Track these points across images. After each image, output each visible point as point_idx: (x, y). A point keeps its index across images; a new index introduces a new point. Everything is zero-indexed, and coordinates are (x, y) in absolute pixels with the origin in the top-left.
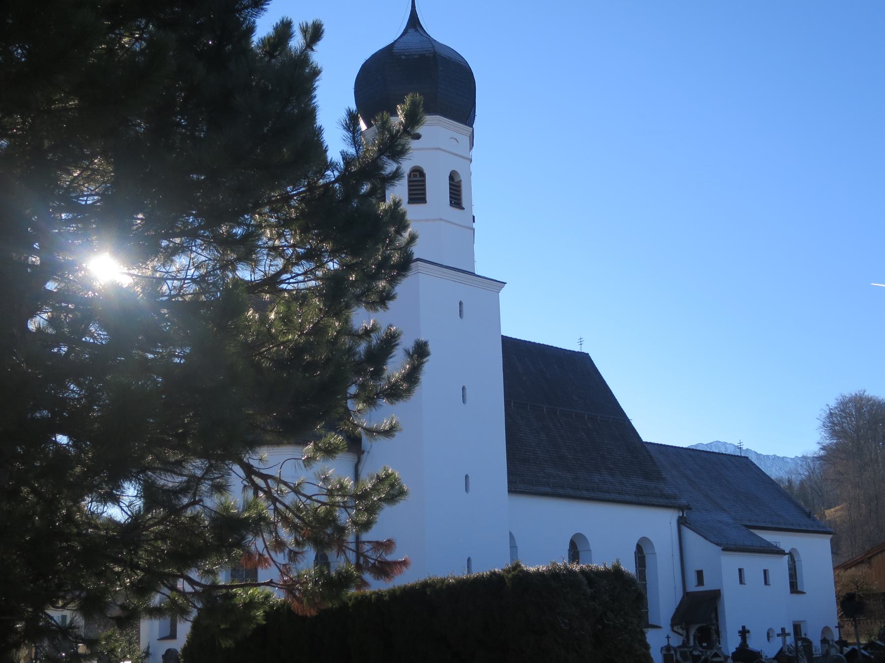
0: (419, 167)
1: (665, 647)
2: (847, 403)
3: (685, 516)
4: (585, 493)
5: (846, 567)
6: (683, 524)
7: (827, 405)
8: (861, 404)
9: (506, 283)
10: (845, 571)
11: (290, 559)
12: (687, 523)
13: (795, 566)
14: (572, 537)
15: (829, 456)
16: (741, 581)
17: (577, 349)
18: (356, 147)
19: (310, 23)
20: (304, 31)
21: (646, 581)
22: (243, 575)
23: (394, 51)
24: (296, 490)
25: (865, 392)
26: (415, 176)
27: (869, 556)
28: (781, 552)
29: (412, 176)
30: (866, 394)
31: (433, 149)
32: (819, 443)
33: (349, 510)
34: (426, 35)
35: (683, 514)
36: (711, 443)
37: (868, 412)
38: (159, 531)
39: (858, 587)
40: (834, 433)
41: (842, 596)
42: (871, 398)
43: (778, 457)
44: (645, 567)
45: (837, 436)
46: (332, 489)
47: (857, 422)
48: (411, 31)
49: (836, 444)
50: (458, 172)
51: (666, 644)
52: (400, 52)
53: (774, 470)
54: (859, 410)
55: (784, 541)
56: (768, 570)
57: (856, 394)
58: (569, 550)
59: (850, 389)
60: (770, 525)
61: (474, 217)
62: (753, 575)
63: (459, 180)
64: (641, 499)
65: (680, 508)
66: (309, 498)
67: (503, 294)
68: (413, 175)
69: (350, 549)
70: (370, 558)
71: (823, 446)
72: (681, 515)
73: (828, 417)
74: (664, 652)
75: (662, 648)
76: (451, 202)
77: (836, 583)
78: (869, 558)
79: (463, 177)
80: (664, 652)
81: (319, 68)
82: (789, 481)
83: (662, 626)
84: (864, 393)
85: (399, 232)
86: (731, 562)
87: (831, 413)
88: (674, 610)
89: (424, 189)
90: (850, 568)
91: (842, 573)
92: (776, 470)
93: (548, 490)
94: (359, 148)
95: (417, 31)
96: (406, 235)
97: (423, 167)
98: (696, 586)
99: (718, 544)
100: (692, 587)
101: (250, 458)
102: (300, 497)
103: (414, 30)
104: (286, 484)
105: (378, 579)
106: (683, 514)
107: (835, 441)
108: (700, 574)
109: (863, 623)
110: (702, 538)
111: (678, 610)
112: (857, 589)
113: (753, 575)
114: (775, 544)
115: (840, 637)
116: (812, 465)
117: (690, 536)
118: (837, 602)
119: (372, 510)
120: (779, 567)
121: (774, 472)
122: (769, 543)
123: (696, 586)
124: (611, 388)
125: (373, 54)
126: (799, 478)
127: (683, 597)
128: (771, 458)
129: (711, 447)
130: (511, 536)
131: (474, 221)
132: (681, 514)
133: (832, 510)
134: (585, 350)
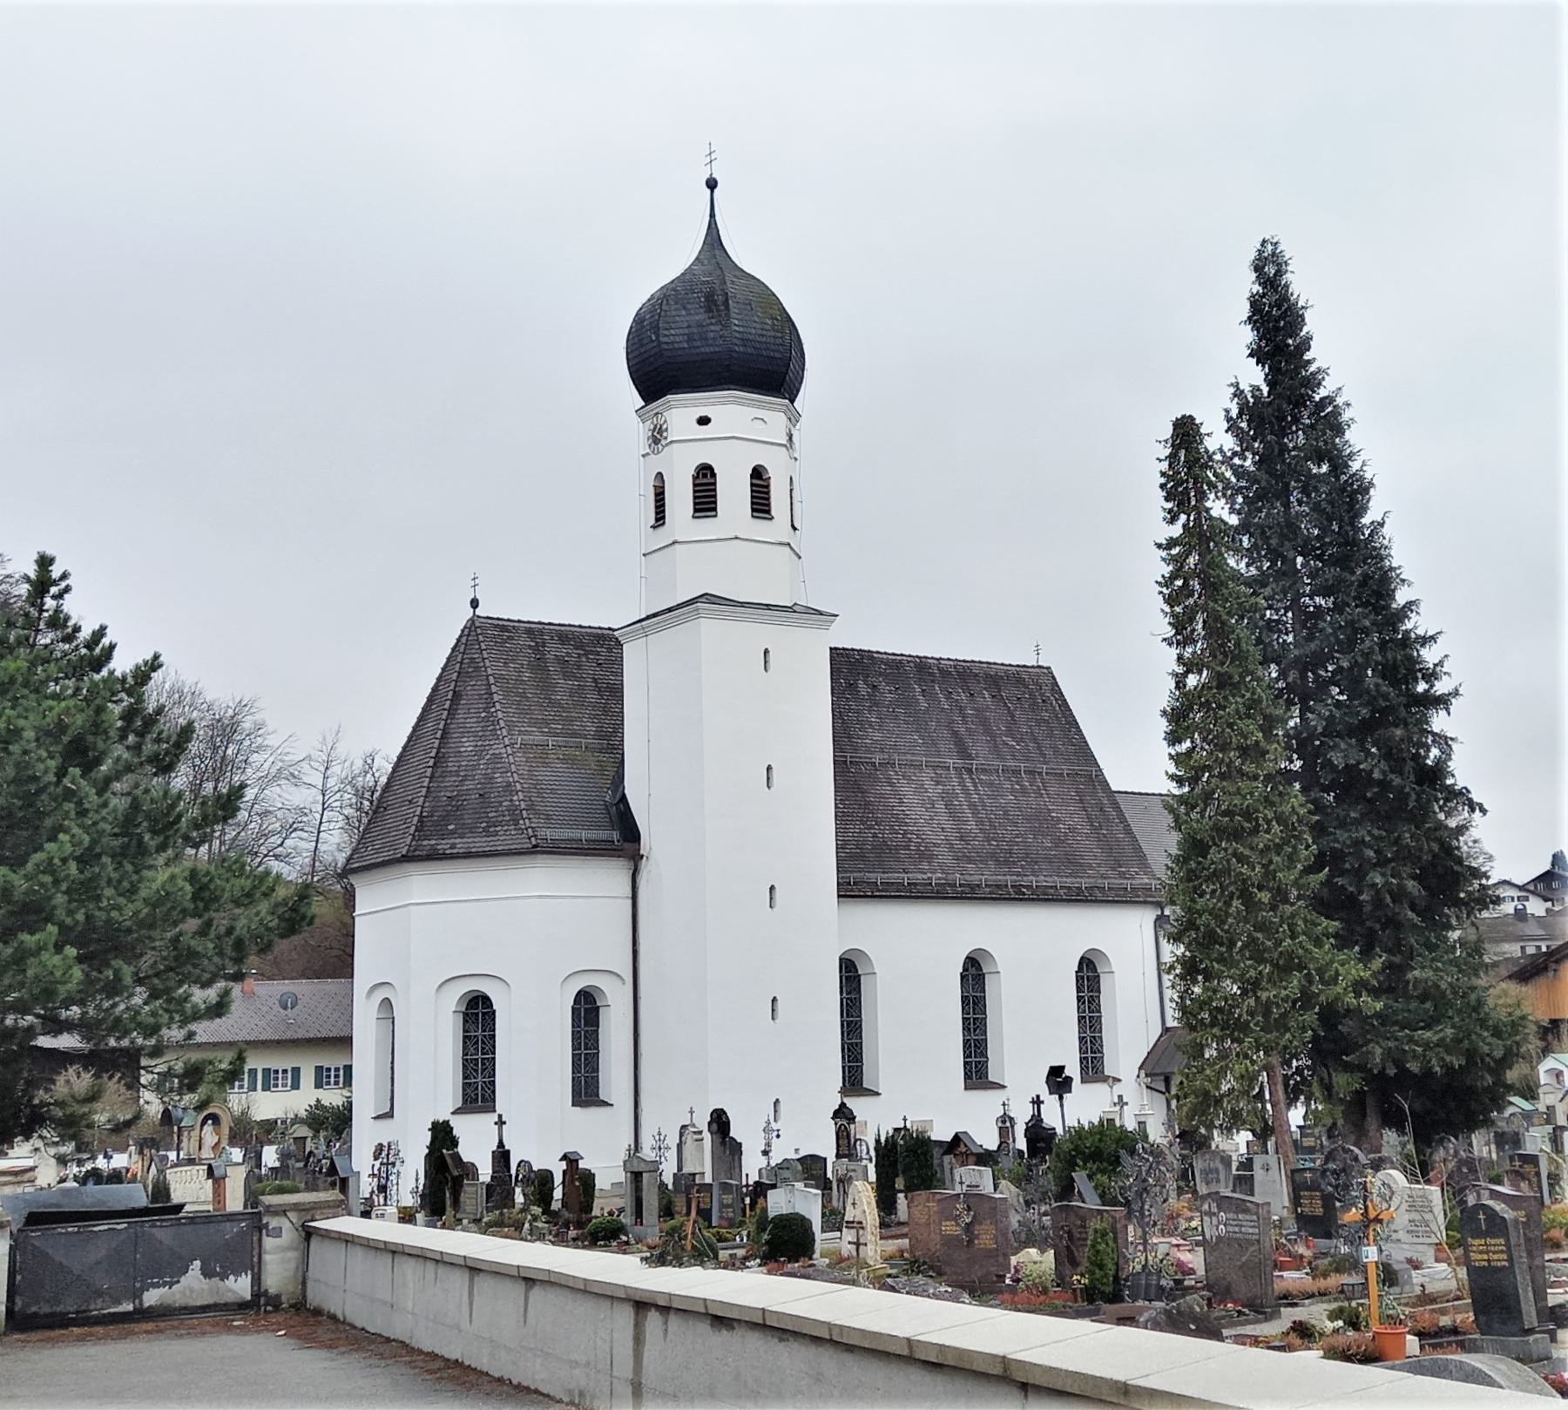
9: (837, 616)
17: (1030, 661)
72: (1159, 913)
132: (1159, 913)
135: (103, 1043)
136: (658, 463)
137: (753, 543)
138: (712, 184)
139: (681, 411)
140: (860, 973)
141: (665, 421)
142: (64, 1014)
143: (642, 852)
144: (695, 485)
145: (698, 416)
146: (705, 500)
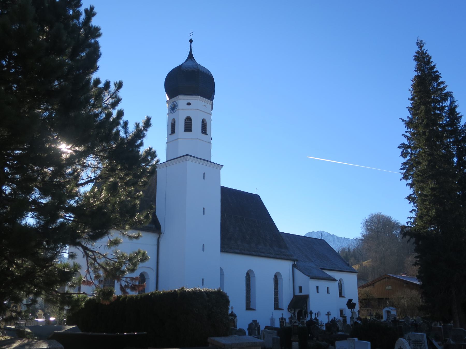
0: (190, 117)
1: (281, 318)
2: (373, 217)
3: (295, 263)
4: (254, 253)
5: (363, 287)
6: (294, 267)
7: (365, 218)
8: (379, 218)
9: (223, 166)
10: (363, 289)
11: (99, 283)
12: (296, 266)
13: (341, 286)
14: (248, 271)
15: (366, 239)
16: (318, 292)
17: (254, 193)
18: (126, 134)
19: (118, 81)
20: (115, 84)
21: (278, 290)
22: (109, 283)
23: (181, 68)
24: (104, 257)
25: (381, 213)
26: (188, 120)
27: (373, 283)
28: (335, 280)
29: (186, 120)
30: (382, 214)
31: (195, 109)
32: (361, 233)
33: (126, 264)
34: (195, 62)
35: (295, 263)
36: (318, 232)
37: (382, 221)
38: (448, 117)
39: (368, 295)
40: (368, 230)
41: (361, 299)
42: (384, 215)
43: (346, 239)
44: (278, 284)
45: (369, 231)
46: (119, 257)
47: (378, 225)
48: (189, 60)
49: (368, 234)
50: (206, 119)
51: (281, 317)
52: (184, 69)
53: (344, 243)
54: (378, 220)
55: (337, 275)
56: (329, 287)
57: (377, 214)
58: (246, 277)
59: (375, 211)
60: (331, 269)
61: (211, 138)
62: (323, 289)
63: (206, 122)
64: (278, 256)
65: (293, 260)
66: (110, 259)
67: (222, 170)
68: (187, 120)
69: (123, 280)
70: (129, 283)
71: (363, 235)
72: (294, 263)
73: (366, 223)
74: (280, 320)
75: (280, 319)
76: (202, 132)
77: (359, 293)
78: (374, 283)
79: (207, 121)
80: (280, 320)
81: (121, 98)
82: (349, 249)
83: (284, 309)
84: (381, 214)
85: (152, 159)
86: (313, 284)
87: (367, 221)
88: (289, 303)
89: (191, 126)
90: (365, 287)
91: (362, 289)
92: (345, 244)
93: (238, 251)
94: (127, 135)
95: (191, 60)
96: (156, 159)
97: (191, 117)
98: (299, 293)
99: (308, 276)
100: (297, 293)
101: (88, 244)
102: (106, 259)
103: (190, 59)
104: (101, 254)
105: (132, 291)
106: (295, 263)
107: (368, 233)
108: (300, 288)
109: (369, 310)
110: (301, 273)
111: (291, 303)
112: (368, 296)
113: (323, 289)
114: (332, 276)
115: (359, 316)
116: (358, 243)
117: (297, 272)
118: (359, 301)
119: (135, 265)
120: (334, 286)
121: (336, 247)
122: (330, 276)
123: (299, 293)
124: (267, 210)
125: (173, 68)
126: (353, 248)
127: (293, 297)
128: (343, 239)
129: (318, 233)
130: (221, 269)
131: (211, 140)
132: (294, 263)
133: (366, 262)
134: (257, 194)
135: (43, 313)
136: (174, 116)
137: (170, 159)
138: (191, 41)
139: (182, 100)
140: (250, 276)
141: (177, 103)
142: (399, 305)
143: (161, 232)
144: (185, 122)
145: (187, 103)
146: (188, 127)
